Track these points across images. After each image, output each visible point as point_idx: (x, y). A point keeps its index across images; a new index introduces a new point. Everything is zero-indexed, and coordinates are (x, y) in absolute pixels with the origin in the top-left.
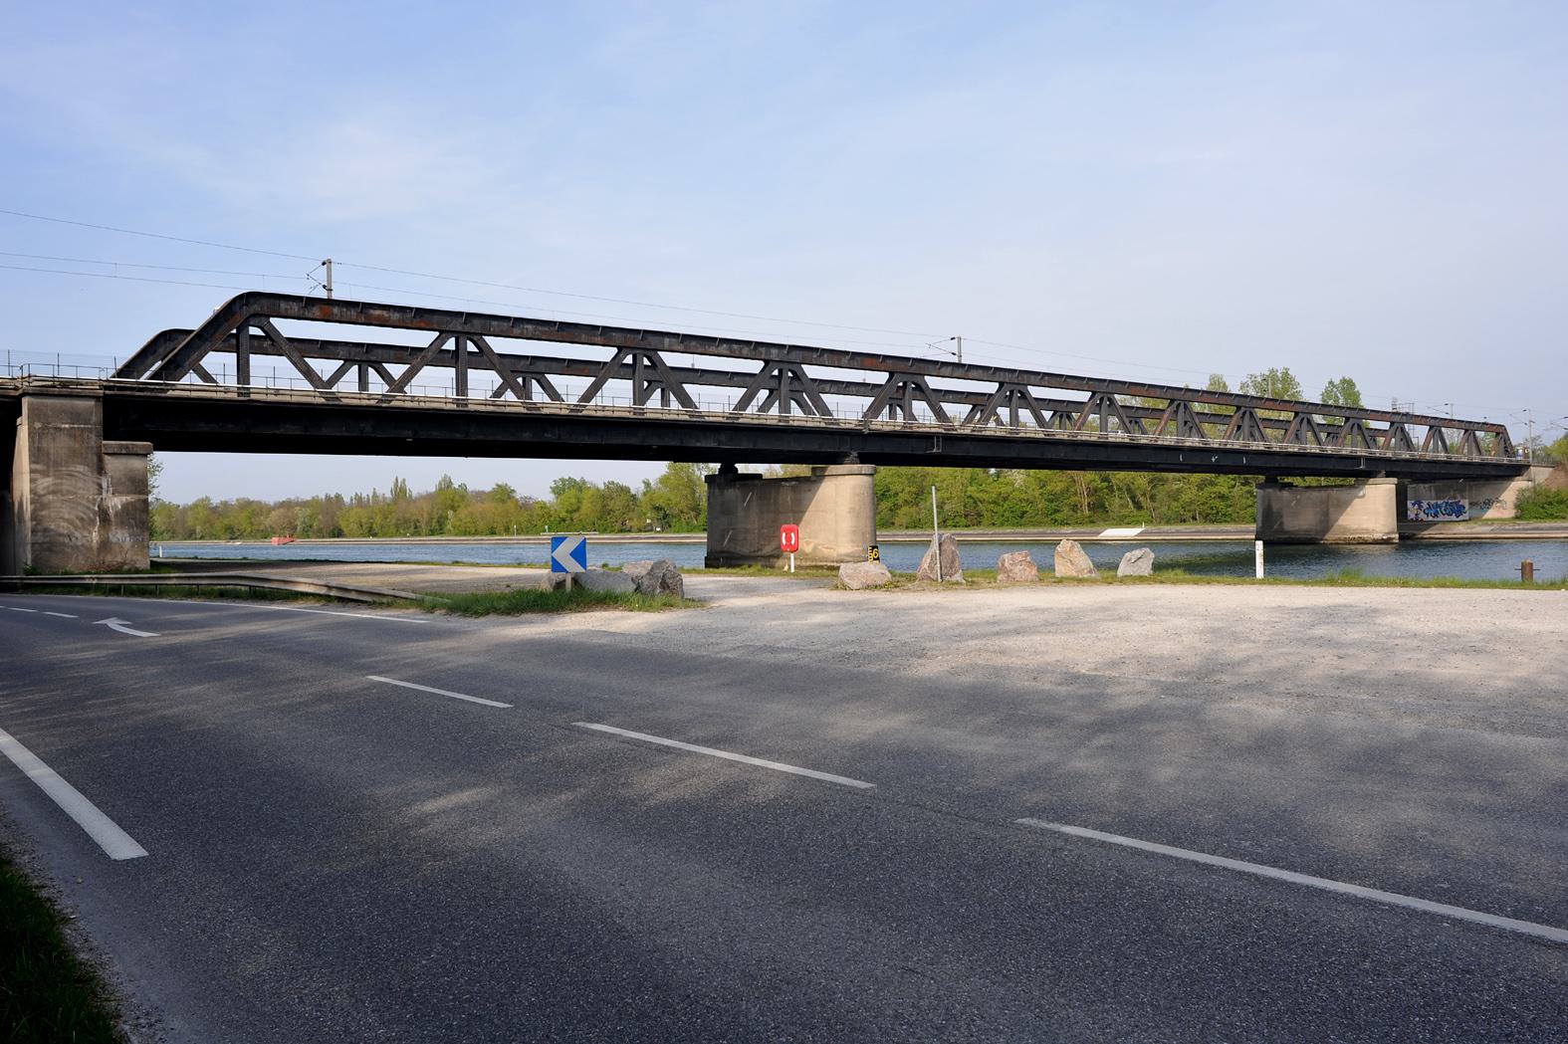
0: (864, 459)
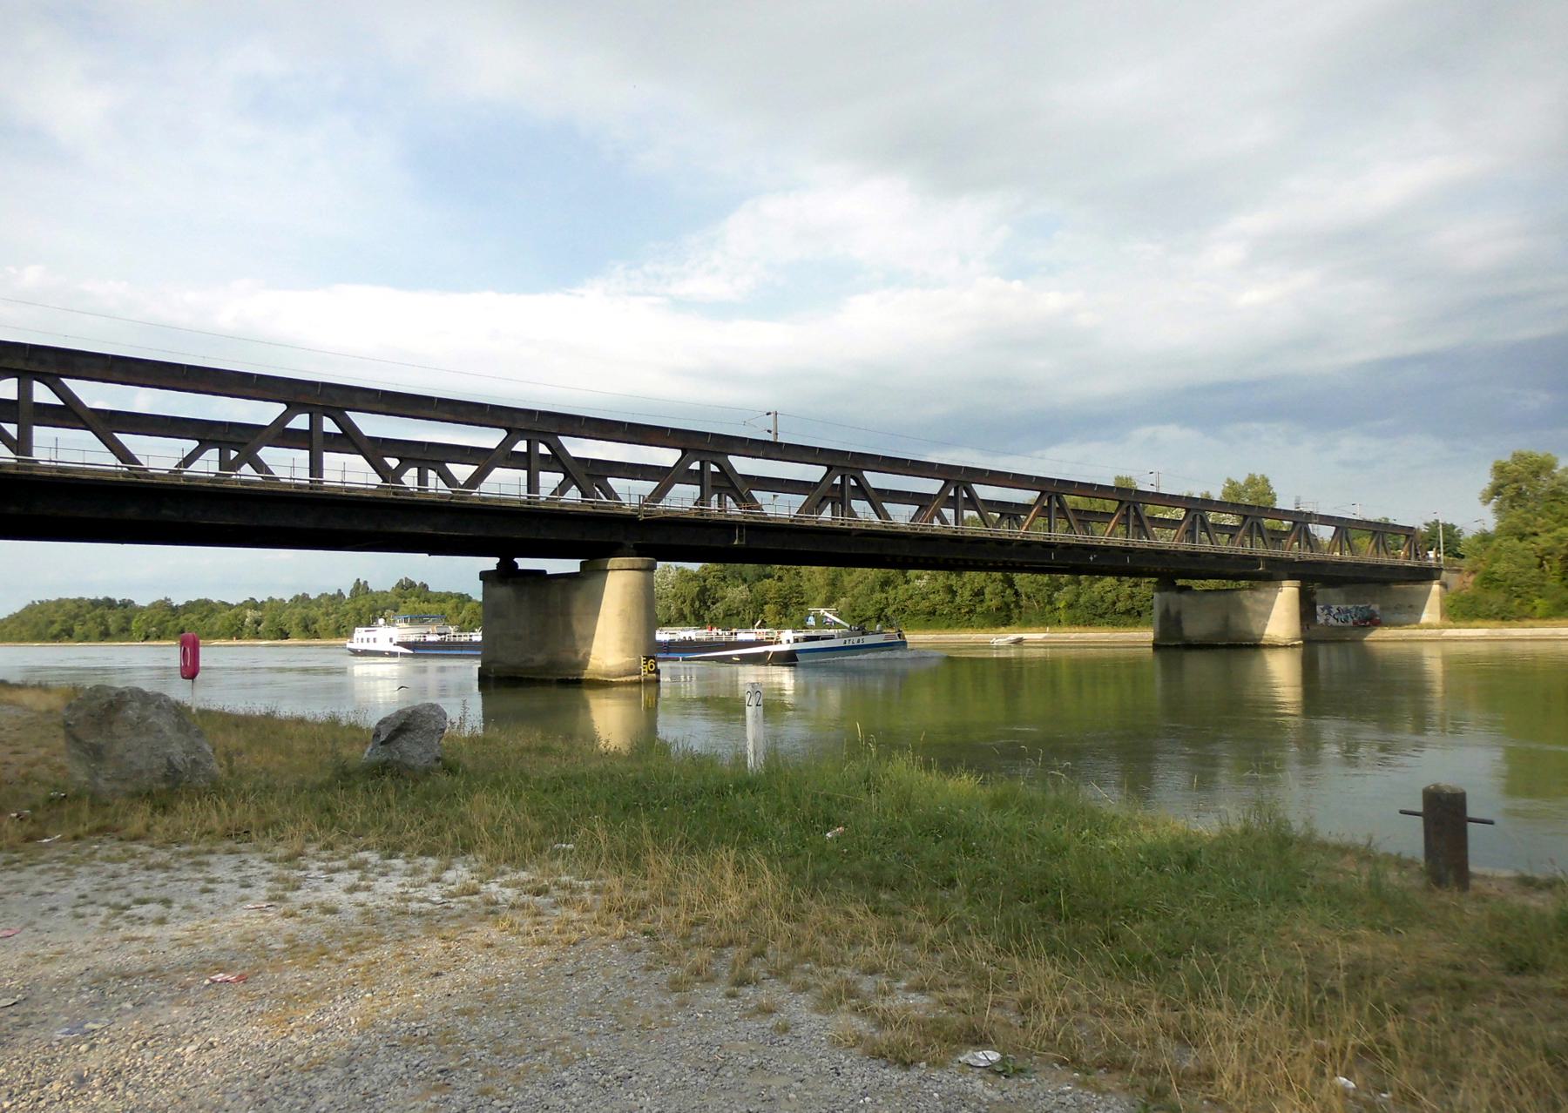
0: (640, 551)
